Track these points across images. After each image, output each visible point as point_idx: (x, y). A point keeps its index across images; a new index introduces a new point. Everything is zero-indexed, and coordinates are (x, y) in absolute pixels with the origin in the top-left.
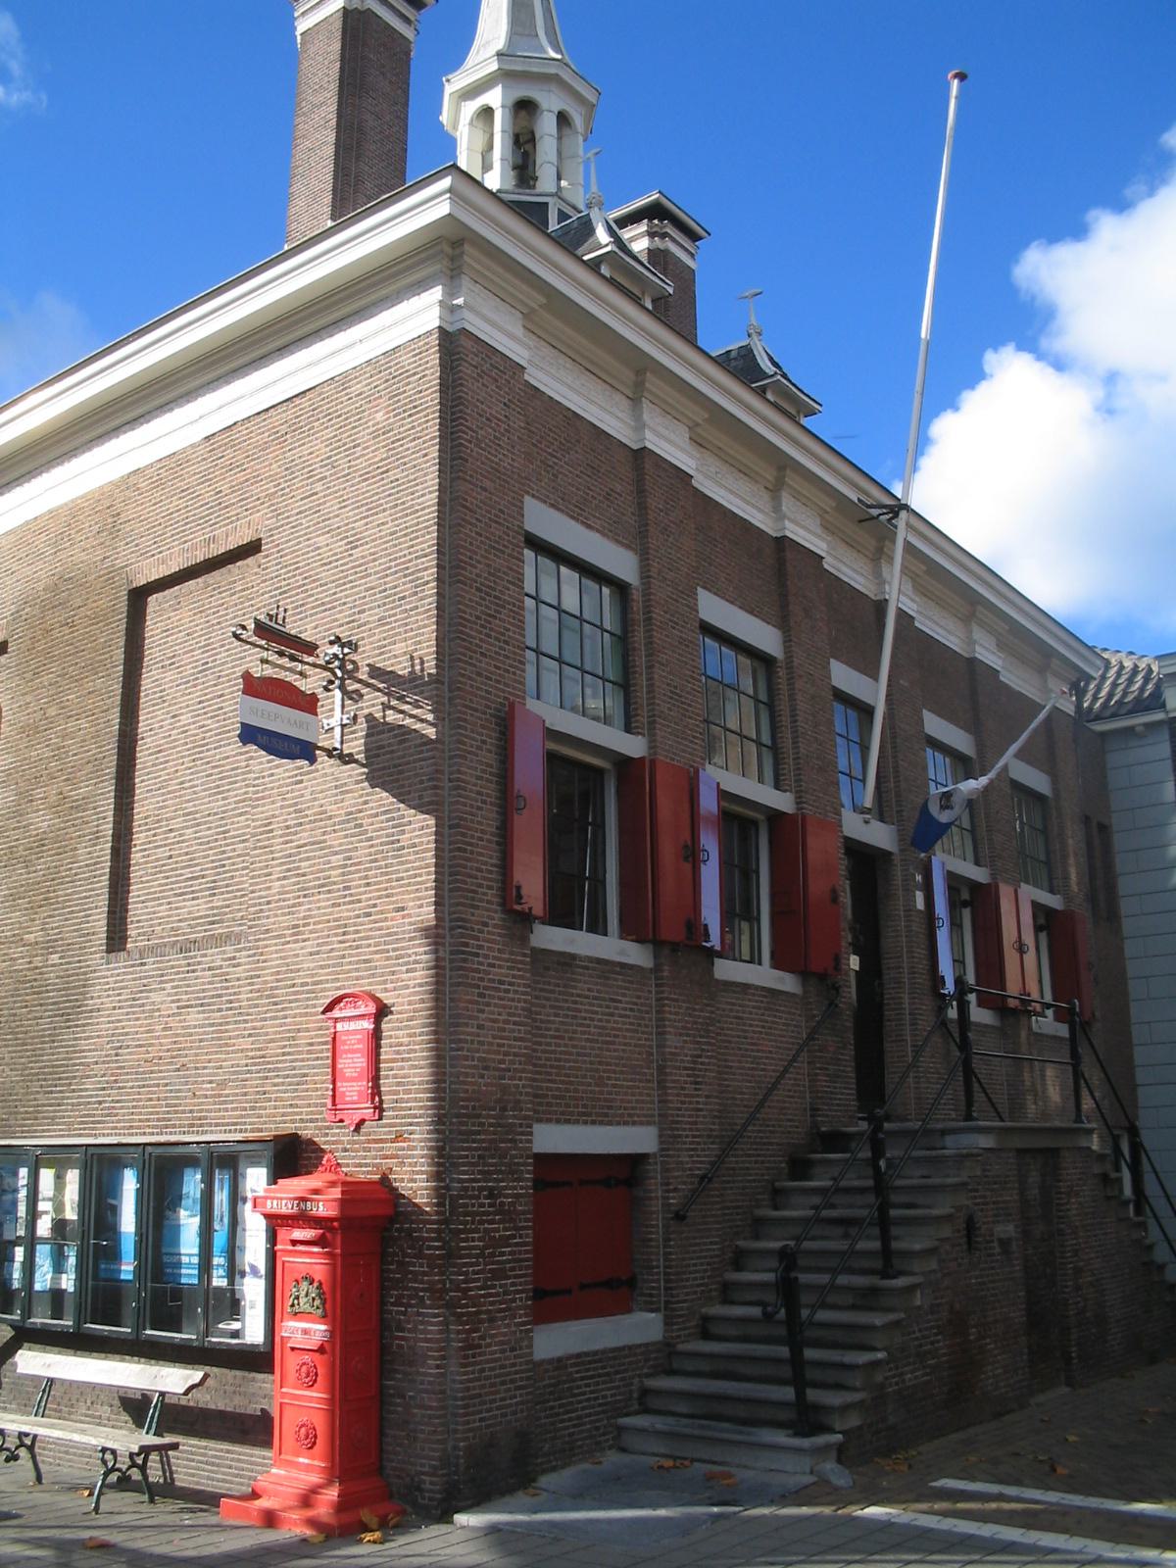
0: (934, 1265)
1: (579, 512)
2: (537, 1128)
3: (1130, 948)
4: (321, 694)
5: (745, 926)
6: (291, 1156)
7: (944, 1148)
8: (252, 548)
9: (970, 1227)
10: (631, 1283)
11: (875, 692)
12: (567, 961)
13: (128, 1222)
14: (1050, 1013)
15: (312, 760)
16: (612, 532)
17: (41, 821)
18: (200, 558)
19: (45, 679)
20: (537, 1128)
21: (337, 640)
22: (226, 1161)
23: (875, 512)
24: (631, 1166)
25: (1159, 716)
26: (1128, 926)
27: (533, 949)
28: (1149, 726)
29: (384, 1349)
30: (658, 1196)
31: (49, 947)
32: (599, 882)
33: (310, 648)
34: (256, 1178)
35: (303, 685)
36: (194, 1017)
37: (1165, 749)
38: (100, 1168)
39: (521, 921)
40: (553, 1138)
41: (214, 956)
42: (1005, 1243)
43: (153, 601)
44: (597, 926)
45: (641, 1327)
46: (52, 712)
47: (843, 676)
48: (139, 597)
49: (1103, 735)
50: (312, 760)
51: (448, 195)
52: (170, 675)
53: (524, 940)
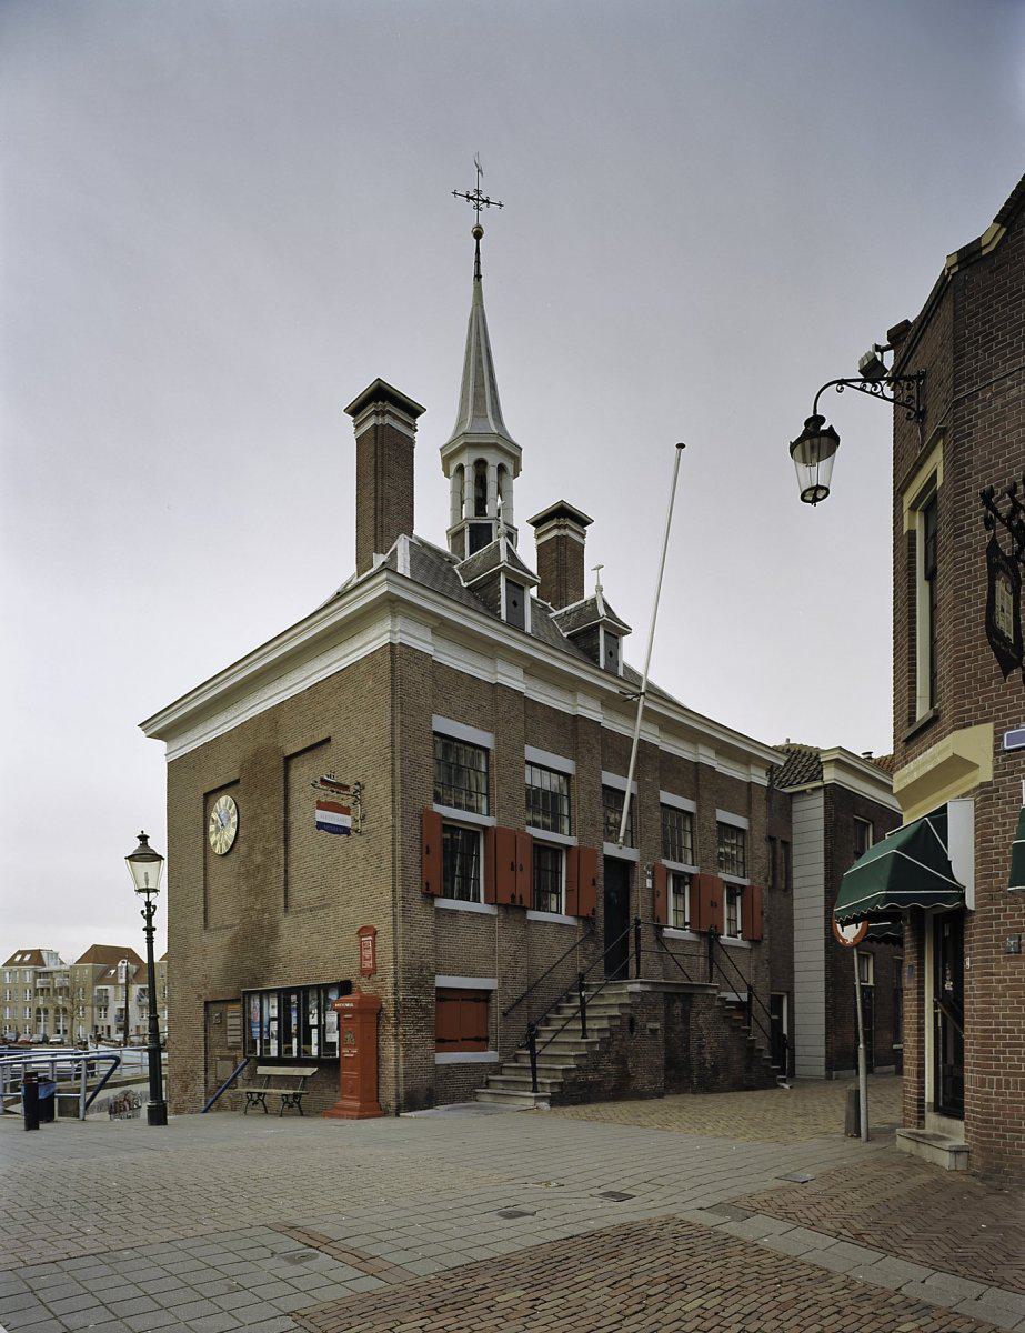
0: (608, 1035)
1: (462, 718)
2: (437, 977)
3: (796, 904)
4: (352, 807)
5: (554, 896)
6: (345, 987)
7: (665, 993)
8: (328, 740)
9: (632, 1022)
10: (487, 1039)
11: (628, 785)
12: (454, 913)
13: (294, 1015)
14: (739, 935)
15: (349, 834)
16: (482, 725)
17: (258, 859)
18: (309, 744)
19: (255, 796)
20: (437, 977)
21: (358, 784)
22: (326, 988)
23: (629, 697)
24: (484, 996)
25: (819, 784)
26: (796, 893)
27: (437, 908)
28: (814, 789)
29: (378, 1058)
30: (497, 1006)
31: (263, 911)
32: (477, 880)
33: (347, 788)
34: (333, 996)
35: (344, 804)
36: (316, 937)
37: (821, 801)
38: (284, 994)
39: (429, 896)
40: (443, 981)
41: (321, 913)
42: (653, 1031)
43: (294, 763)
44: (476, 899)
45: (490, 1056)
46: (259, 811)
47: (610, 779)
48: (288, 759)
49: (791, 794)
50: (349, 834)
51: (384, 575)
52: (302, 796)
53: (432, 904)
